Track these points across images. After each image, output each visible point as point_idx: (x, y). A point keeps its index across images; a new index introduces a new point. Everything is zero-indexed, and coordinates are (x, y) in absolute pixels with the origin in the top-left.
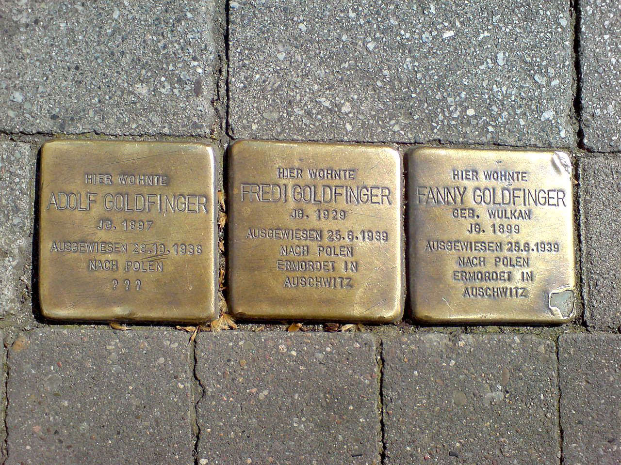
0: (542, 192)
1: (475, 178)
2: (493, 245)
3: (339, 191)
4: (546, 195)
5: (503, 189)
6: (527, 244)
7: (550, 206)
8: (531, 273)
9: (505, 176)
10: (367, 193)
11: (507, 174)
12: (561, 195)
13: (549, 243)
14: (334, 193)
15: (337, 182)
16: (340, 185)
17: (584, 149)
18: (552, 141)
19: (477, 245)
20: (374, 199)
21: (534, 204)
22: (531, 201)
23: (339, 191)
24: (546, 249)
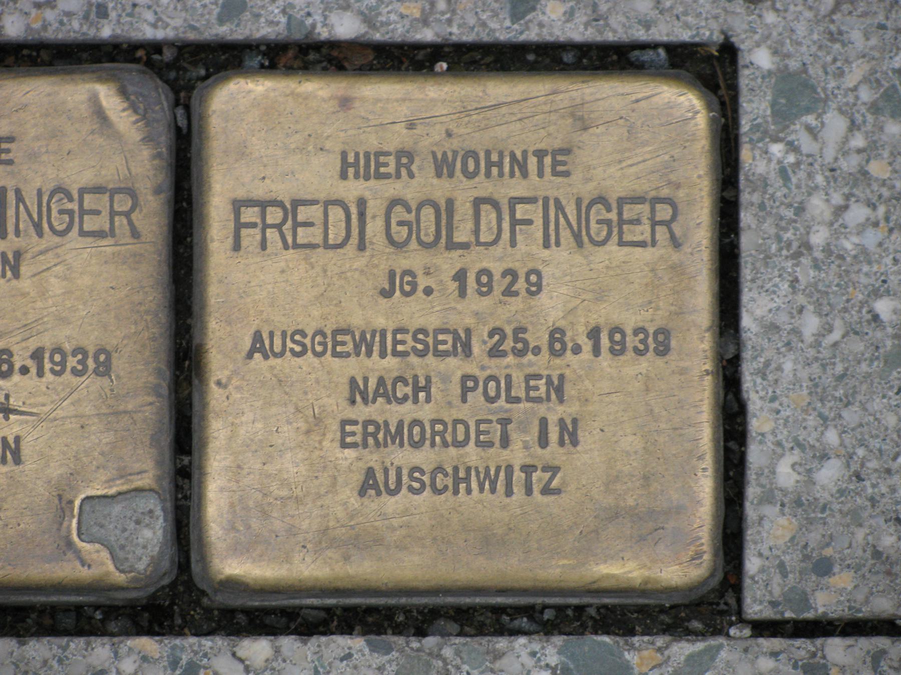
0: (399, 209)
1: (404, 172)
2: (348, 338)
3: (521, 211)
4: (74, 206)
5: (478, 203)
6: (557, 335)
7: (626, 249)
8: (353, 402)
9: (500, 165)
10: (69, 206)
11: (507, 160)
12: (123, 203)
13: (80, 350)
14: (506, 218)
15: (518, 188)
16: (525, 194)
17: (860, 82)
18: (458, 12)
19: (340, 338)
20: (90, 223)
21: (32, 230)
22: (565, 234)
23: (521, 211)
24: (69, 366)
